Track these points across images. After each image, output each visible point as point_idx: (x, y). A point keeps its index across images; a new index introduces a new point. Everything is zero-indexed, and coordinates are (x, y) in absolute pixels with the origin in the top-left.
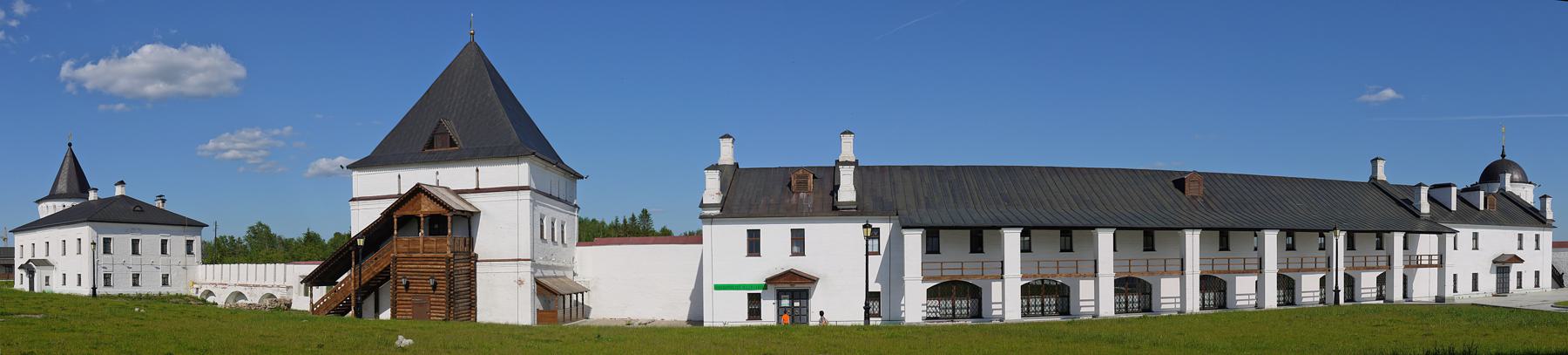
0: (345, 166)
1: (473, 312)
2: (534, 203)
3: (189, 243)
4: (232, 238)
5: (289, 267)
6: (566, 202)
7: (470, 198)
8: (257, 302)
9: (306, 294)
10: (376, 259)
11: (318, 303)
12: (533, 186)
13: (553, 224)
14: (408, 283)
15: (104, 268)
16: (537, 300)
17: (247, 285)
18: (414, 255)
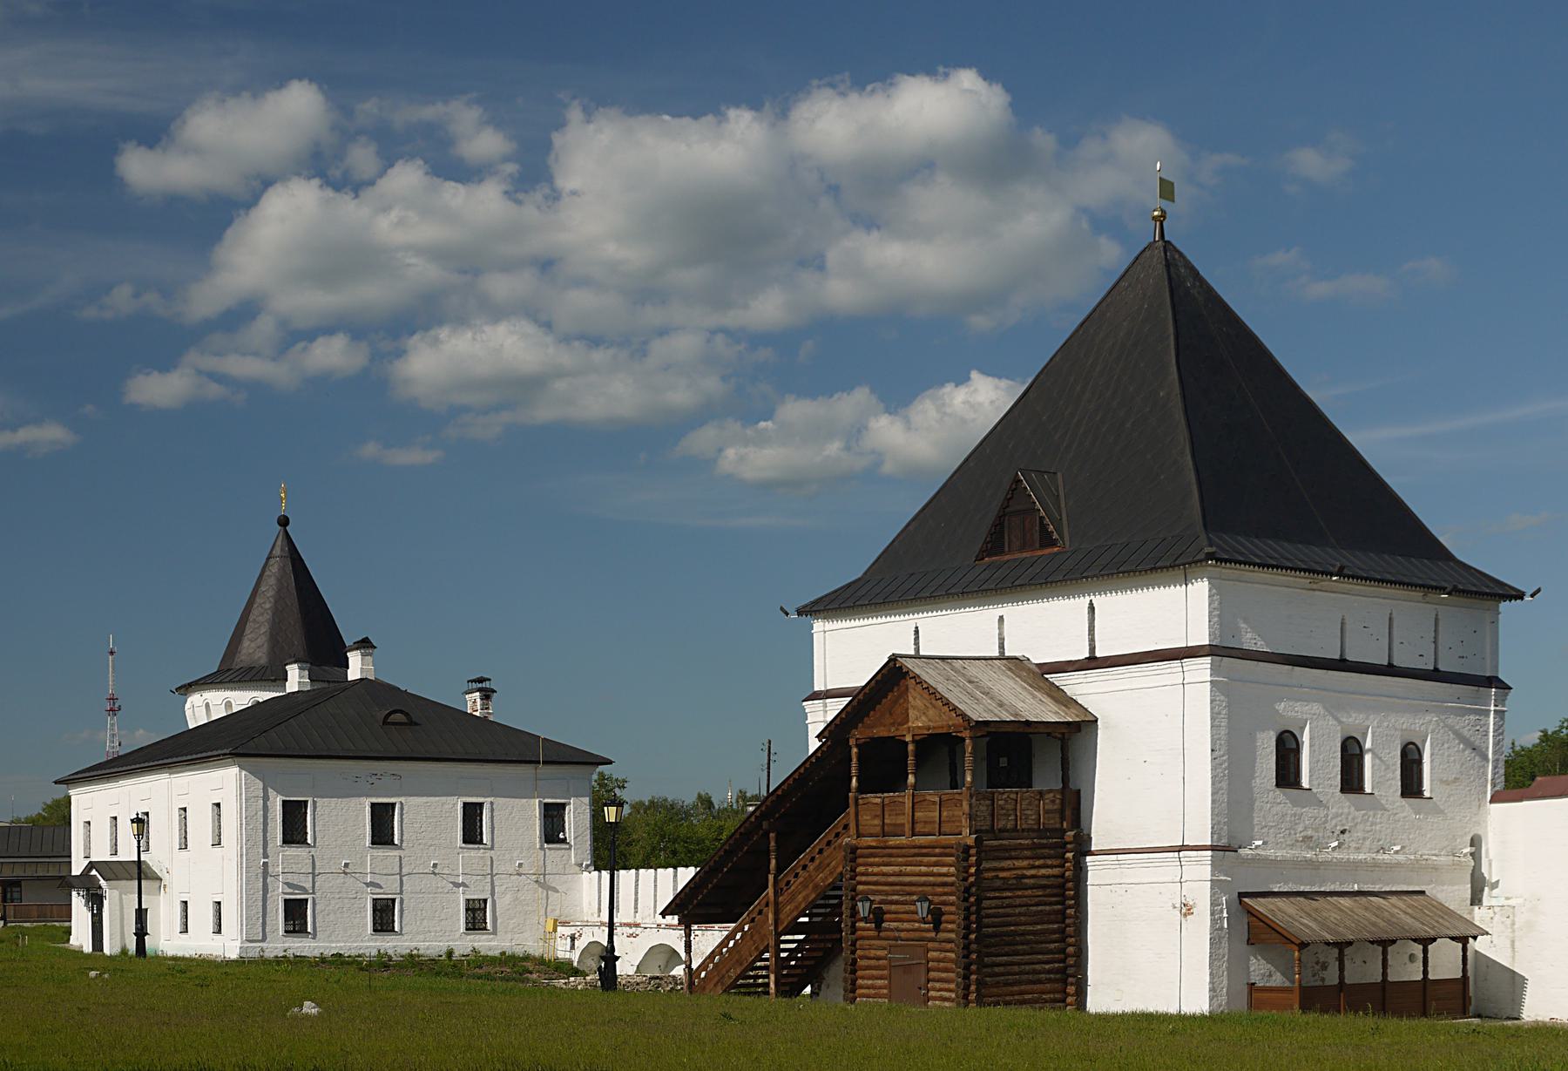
0: (791, 609)
3: (553, 819)
7: (1072, 684)
10: (821, 852)
11: (703, 966)
15: (371, 884)
18: (893, 841)
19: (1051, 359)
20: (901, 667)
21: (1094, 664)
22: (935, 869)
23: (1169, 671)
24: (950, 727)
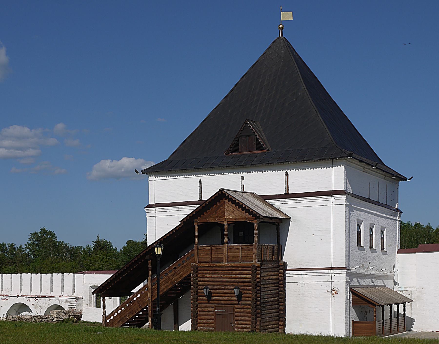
1: (281, 323)
2: (350, 208)
4: (12, 246)
5: (79, 277)
6: (386, 206)
7: (278, 204)
8: (42, 314)
9: (98, 305)
10: (175, 268)
11: (112, 314)
12: (350, 190)
13: (371, 230)
14: (210, 293)
16: (352, 311)
17: (31, 296)
18: (217, 264)
19: (241, 79)
20: (225, 194)
21: (288, 196)
22: (239, 276)
23: (325, 199)
24: (247, 219)
